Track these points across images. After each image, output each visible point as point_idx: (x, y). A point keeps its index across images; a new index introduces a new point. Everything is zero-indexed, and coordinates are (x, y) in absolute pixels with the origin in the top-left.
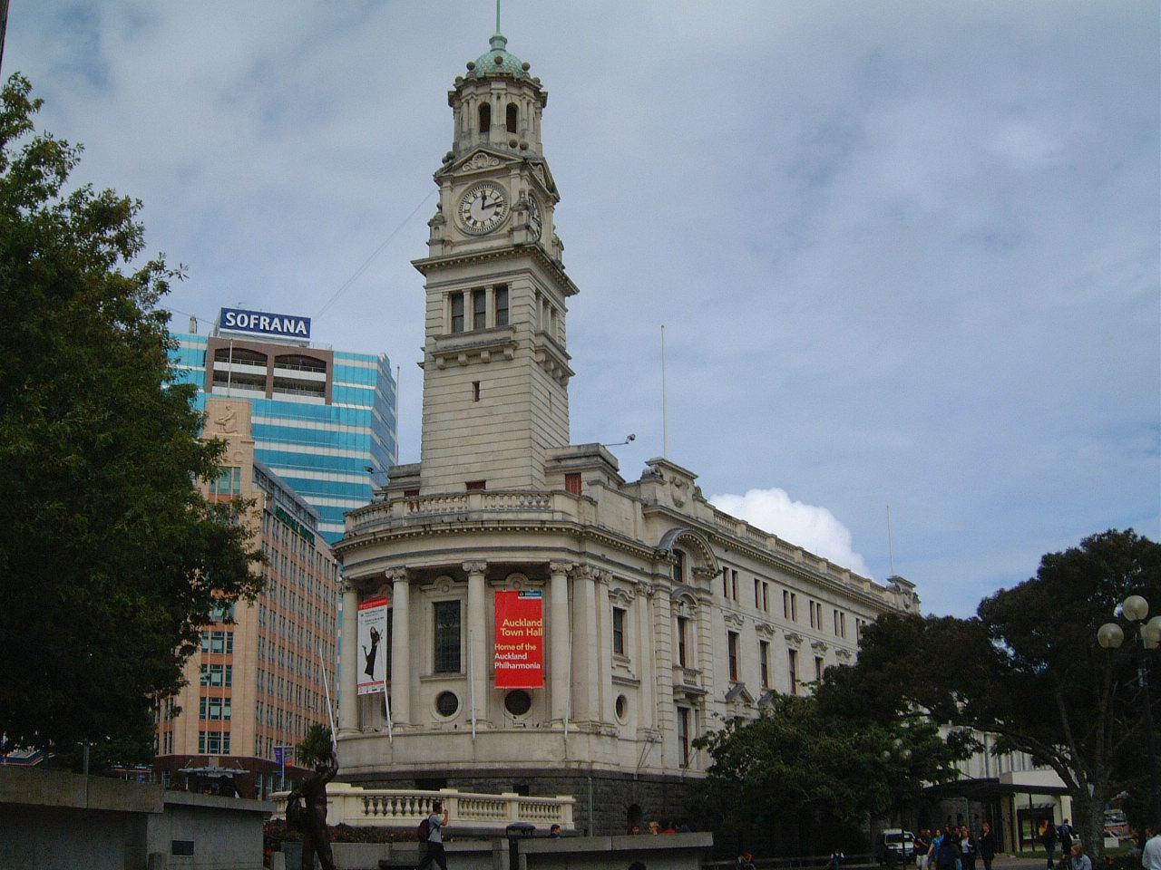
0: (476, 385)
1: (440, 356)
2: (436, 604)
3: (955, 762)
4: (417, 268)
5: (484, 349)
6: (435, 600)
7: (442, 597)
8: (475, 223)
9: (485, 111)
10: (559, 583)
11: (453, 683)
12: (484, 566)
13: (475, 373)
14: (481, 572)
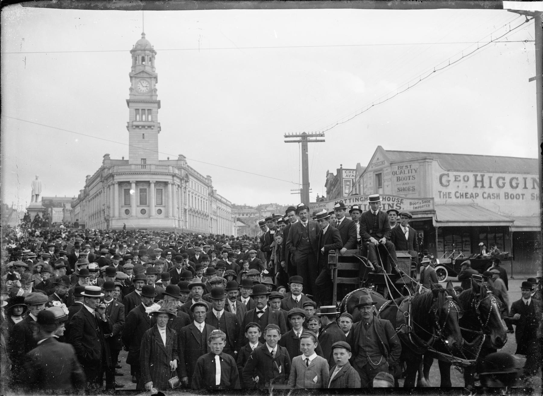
13: (143, 131)
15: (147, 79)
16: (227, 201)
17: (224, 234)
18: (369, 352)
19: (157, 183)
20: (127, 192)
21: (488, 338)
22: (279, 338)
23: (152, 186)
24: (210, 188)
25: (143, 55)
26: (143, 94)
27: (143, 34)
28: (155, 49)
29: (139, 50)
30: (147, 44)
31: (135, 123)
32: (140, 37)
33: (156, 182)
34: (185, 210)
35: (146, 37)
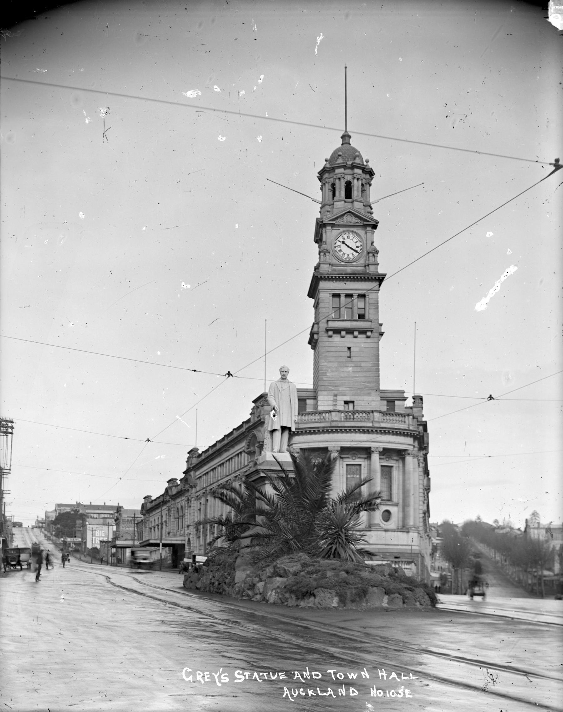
0: (349, 348)
2: (347, 465)
13: (349, 340)
15: (355, 230)
18: (205, 539)
19: (386, 453)
22: (227, 556)
23: (375, 457)
25: (349, 178)
26: (349, 263)
27: (346, 137)
28: (371, 165)
29: (339, 167)
30: (355, 154)
32: (338, 143)
33: (384, 449)
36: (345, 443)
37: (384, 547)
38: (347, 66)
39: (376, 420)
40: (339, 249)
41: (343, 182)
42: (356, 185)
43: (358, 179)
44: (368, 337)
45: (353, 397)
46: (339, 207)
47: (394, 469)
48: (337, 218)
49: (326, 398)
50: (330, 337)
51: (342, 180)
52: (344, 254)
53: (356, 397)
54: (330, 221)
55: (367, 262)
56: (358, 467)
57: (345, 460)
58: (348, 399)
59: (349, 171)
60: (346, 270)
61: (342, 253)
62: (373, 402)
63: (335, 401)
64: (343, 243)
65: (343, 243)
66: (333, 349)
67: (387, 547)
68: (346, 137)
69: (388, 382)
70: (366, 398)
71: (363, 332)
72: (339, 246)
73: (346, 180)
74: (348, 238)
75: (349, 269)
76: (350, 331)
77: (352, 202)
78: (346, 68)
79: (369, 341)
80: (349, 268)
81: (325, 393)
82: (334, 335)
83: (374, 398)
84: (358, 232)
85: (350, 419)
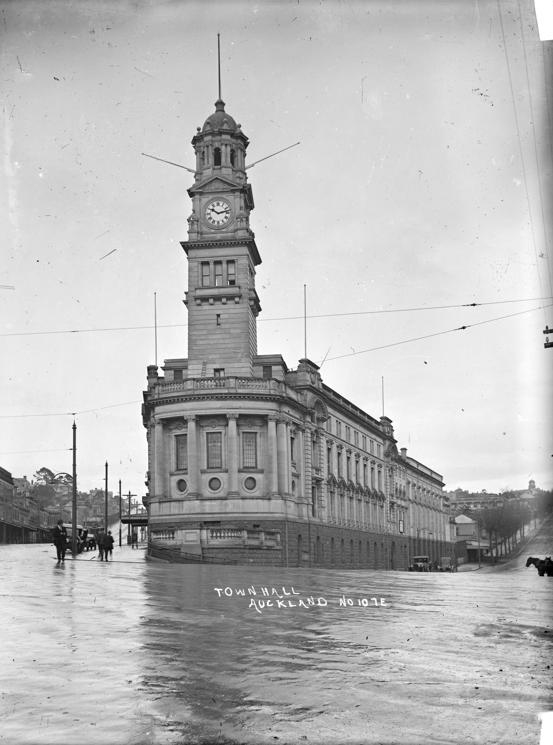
0: (218, 316)
1: (198, 299)
3: (300, 516)
4: (183, 246)
5: (211, 298)
6: (176, 434)
7: (178, 432)
8: (218, 222)
9: (217, 154)
10: (272, 425)
11: (218, 474)
12: (194, 417)
13: (218, 308)
14: (193, 420)
15: (224, 196)
16: (432, 472)
17: (541, 574)
19: (243, 419)
20: (181, 440)
21: (266, 604)
24: (388, 443)
25: (217, 145)
26: (219, 229)
27: (220, 104)
31: (200, 293)
34: (317, 482)
35: (226, 108)
36: (201, 411)
37: (269, 515)
38: (220, 33)
39: (232, 386)
40: (209, 216)
41: (211, 151)
42: (225, 152)
43: (226, 145)
44: (237, 303)
45: (223, 364)
46: (207, 174)
47: (258, 435)
48: (205, 186)
49: (196, 367)
50: (199, 305)
51: (210, 147)
52: (214, 221)
53: (226, 365)
54: (198, 189)
55: (236, 227)
56: (254, 436)
57: (205, 428)
58: (217, 366)
59: (218, 138)
60: (216, 237)
61: (212, 220)
62: (243, 369)
63: (204, 369)
64: (213, 210)
65: (213, 210)
66: (203, 317)
67: (245, 515)
68: (220, 104)
69: (264, 349)
70: (236, 365)
71: (230, 298)
72: (210, 214)
73: (214, 147)
74: (218, 204)
75: (218, 236)
76: (217, 298)
77: (220, 169)
78: (219, 35)
79: (238, 307)
80: (219, 235)
81: (195, 362)
82: (203, 304)
83: (244, 365)
84: (227, 198)
85: (220, 386)
